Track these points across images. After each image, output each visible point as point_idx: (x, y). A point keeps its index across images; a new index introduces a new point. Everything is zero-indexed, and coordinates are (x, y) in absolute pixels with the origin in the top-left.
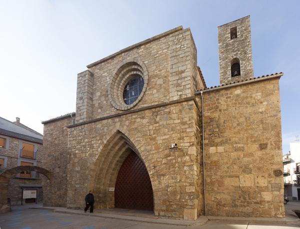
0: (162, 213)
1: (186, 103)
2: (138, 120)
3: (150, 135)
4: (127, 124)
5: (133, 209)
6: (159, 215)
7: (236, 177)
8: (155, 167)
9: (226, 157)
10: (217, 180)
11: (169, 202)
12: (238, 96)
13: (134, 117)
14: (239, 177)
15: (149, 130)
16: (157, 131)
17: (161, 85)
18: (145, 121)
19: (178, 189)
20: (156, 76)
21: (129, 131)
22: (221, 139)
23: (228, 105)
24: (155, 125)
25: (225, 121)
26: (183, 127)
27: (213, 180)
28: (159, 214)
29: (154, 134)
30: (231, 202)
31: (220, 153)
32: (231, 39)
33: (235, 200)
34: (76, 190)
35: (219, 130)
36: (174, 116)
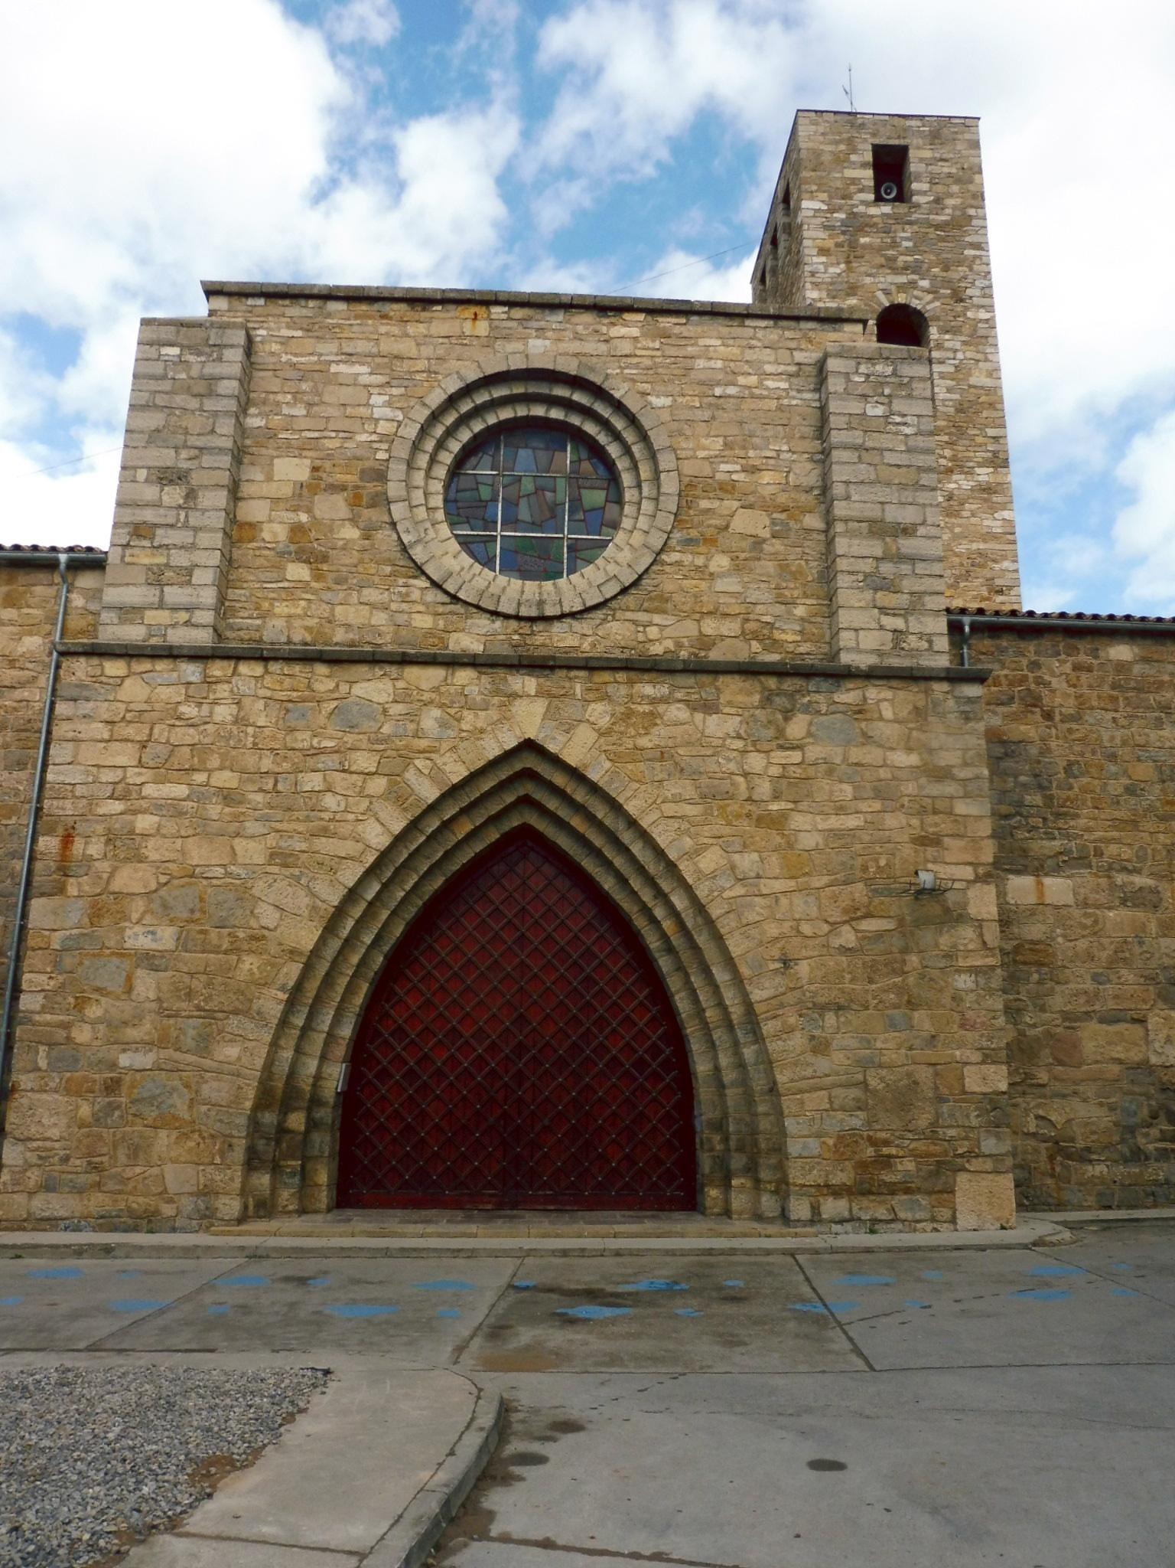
0: (832, 1207)
1: (945, 686)
2: (677, 712)
3: (749, 799)
4: (604, 722)
5: (456, 1204)
6: (816, 1218)
7: (1134, 1021)
8: (786, 962)
9: (1084, 927)
10: (1049, 1034)
11: (873, 1142)
12: (1122, 667)
13: (649, 690)
14: (1142, 1021)
15: (745, 775)
16: (794, 786)
17: (758, 543)
18: (716, 726)
19: (924, 1074)
20: (727, 488)
21: (614, 758)
22: (1056, 845)
23: (1082, 702)
24: (779, 756)
25: (1070, 764)
26: (935, 789)
27: (1031, 1032)
28: (815, 1209)
29: (776, 796)
30: (1116, 1138)
31: (1057, 907)
32: (879, 199)
33: (1131, 1130)
34: (112, 1087)
35: (1049, 799)
36: (886, 731)
